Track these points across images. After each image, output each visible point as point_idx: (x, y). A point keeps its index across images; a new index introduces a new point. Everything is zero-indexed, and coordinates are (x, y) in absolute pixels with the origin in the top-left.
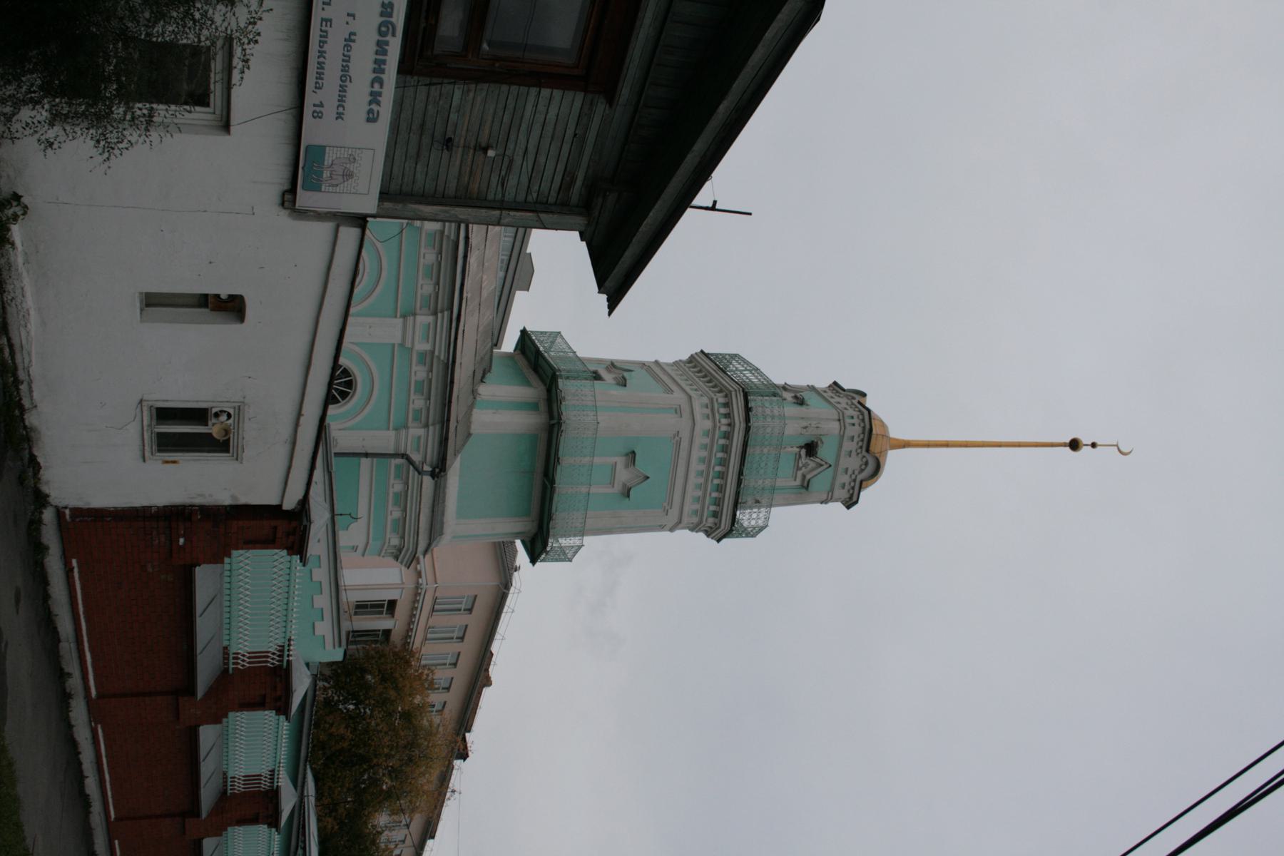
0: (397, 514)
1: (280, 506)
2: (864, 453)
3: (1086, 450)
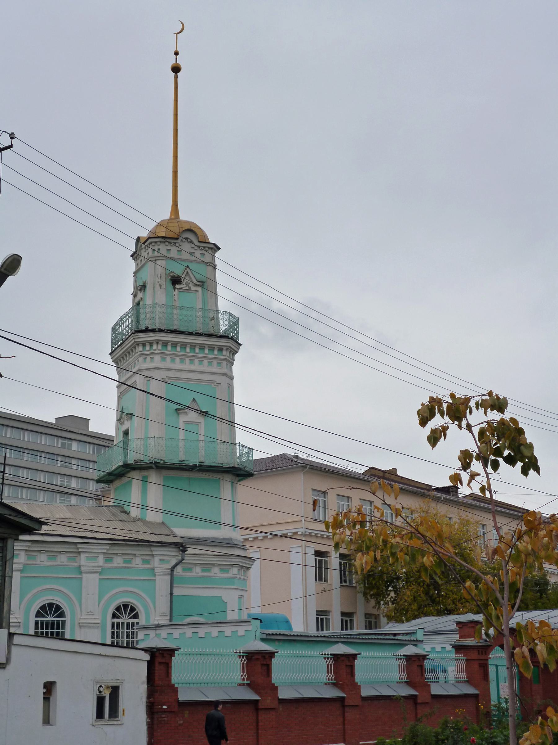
0: (216, 570)
1: (148, 661)
2: (179, 241)
3: (181, 62)
